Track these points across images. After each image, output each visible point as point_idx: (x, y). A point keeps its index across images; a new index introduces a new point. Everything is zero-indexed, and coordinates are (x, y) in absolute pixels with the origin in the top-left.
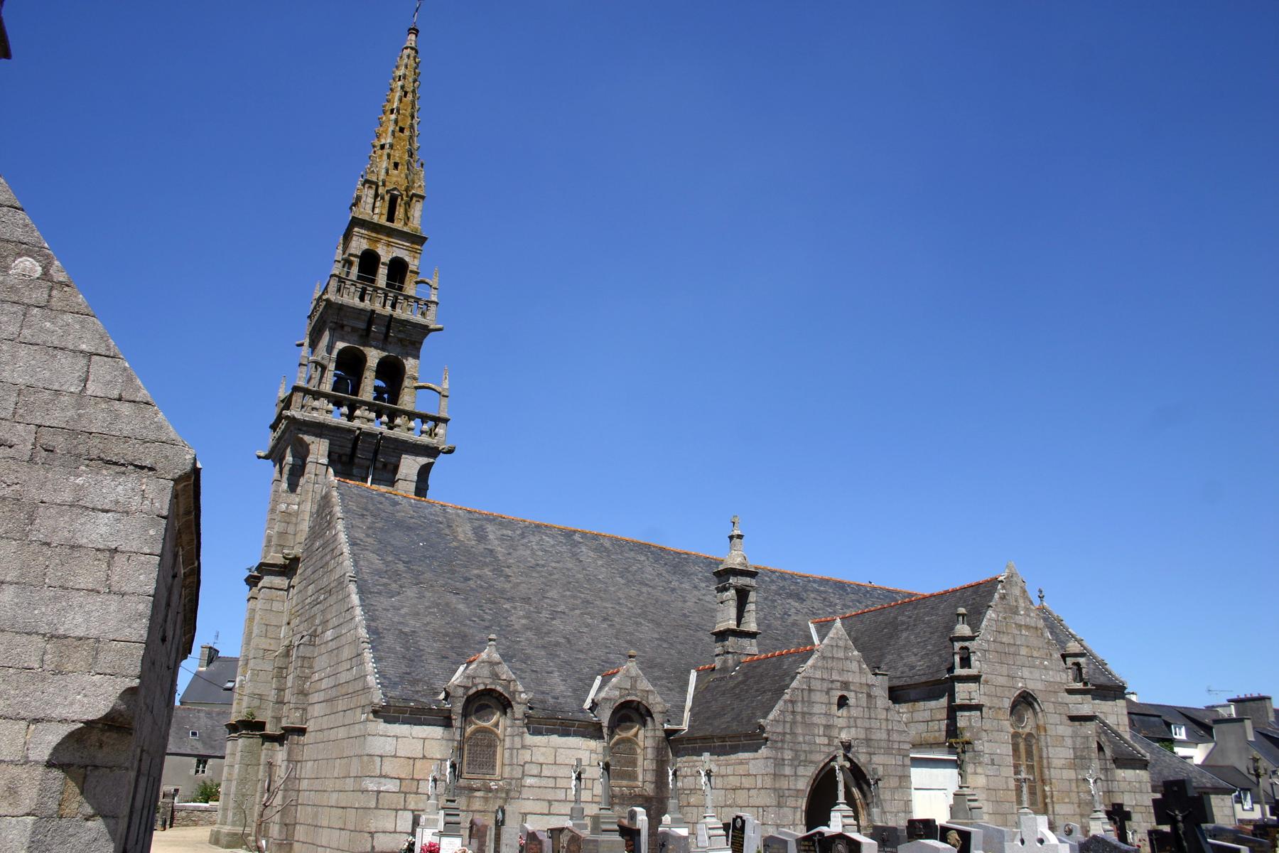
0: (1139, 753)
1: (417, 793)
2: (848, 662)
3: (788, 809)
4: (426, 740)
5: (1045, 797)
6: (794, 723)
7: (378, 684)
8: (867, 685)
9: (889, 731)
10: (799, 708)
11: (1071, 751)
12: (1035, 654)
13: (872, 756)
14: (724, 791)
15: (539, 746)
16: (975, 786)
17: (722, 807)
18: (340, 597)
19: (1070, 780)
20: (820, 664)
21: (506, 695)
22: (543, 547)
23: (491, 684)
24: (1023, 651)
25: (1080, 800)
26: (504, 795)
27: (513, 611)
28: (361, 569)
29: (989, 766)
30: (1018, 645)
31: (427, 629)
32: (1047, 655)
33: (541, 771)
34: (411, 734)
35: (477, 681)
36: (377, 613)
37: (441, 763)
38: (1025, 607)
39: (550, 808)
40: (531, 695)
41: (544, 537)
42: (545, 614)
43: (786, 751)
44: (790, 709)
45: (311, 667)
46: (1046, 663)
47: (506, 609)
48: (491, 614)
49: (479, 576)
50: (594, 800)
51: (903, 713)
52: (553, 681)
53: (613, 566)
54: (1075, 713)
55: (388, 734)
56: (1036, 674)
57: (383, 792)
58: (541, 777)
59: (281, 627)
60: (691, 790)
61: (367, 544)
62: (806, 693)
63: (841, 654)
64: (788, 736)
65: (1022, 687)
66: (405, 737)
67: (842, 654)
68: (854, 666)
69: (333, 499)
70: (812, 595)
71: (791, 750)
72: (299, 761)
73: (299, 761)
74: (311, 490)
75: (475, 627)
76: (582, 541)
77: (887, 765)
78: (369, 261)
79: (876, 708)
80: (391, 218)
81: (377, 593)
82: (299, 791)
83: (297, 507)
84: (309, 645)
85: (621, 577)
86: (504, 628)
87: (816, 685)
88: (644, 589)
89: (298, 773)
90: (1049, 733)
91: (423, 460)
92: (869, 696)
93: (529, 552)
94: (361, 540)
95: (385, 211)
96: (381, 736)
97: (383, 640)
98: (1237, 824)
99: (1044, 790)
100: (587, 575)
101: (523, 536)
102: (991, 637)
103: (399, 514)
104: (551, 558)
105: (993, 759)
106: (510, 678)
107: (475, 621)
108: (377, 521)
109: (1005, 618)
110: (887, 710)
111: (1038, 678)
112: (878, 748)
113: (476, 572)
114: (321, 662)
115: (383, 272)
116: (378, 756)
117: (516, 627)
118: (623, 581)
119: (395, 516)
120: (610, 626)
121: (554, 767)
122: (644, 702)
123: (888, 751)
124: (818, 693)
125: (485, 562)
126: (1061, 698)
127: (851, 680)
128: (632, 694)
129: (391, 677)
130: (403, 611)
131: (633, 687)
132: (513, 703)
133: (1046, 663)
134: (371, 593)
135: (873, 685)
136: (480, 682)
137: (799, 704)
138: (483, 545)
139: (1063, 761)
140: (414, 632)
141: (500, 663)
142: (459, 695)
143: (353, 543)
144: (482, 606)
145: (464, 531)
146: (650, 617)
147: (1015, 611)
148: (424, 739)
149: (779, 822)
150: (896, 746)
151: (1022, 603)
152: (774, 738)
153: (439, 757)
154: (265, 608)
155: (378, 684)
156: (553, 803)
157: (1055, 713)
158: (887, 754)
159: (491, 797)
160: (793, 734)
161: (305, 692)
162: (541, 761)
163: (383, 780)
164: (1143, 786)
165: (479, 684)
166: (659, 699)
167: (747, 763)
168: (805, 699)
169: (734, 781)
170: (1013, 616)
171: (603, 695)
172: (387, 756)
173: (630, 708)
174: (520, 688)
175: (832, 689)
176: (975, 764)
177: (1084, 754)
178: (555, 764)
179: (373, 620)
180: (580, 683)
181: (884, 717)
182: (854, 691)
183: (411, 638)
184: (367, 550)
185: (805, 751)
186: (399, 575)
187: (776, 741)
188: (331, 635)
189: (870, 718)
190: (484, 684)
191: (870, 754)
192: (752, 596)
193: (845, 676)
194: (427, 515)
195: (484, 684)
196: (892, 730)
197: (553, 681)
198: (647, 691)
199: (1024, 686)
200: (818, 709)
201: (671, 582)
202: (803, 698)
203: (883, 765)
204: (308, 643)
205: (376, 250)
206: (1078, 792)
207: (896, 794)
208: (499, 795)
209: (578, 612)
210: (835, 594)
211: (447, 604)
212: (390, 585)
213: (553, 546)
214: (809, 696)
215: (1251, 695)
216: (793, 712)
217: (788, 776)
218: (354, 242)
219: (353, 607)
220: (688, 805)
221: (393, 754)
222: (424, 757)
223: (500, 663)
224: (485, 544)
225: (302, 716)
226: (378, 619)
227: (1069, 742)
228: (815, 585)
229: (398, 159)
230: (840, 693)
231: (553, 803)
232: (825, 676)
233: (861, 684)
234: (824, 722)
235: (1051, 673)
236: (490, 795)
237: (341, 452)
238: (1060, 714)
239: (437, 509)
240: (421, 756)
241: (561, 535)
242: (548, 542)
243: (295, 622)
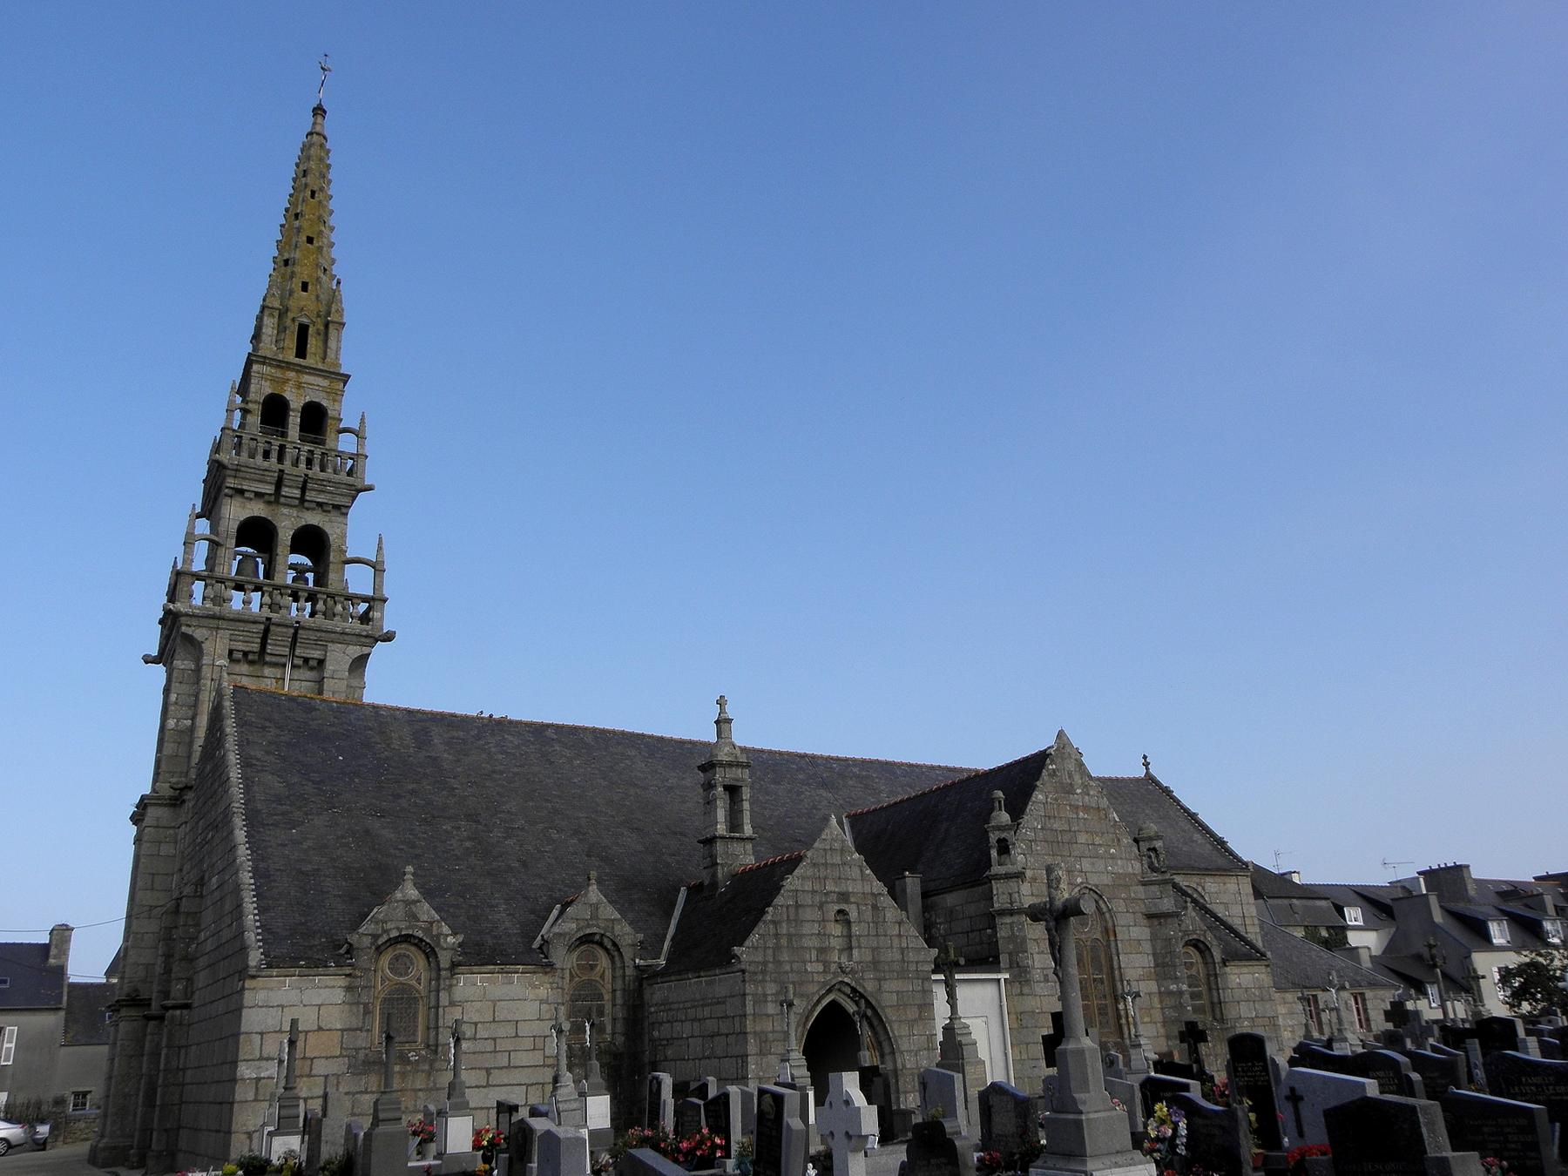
0: (1258, 952)
1: (310, 1076)
2: (847, 868)
3: (773, 1056)
4: (322, 1008)
5: (1119, 1017)
6: (777, 948)
7: (259, 941)
8: (873, 894)
9: (902, 950)
10: (784, 929)
11: (1151, 958)
12: (1098, 840)
13: (882, 982)
14: (701, 1039)
15: (472, 1001)
16: (1022, 1010)
17: (700, 1059)
18: (225, 834)
19: (1150, 994)
20: (809, 873)
21: (428, 941)
22: (505, 748)
23: (407, 928)
24: (1082, 838)
25: (1164, 1018)
26: (427, 1067)
27: (455, 832)
28: (254, 797)
29: (1042, 984)
30: (1075, 832)
31: (337, 864)
33: (476, 1033)
34: (302, 1002)
35: (390, 925)
36: (270, 850)
37: (343, 1034)
38: (1082, 784)
39: (488, 1078)
40: (460, 938)
41: (506, 736)
42: (497, 834)
43: (768, 984)
44: (772, 931)
45: (197, 925)
46: (1112, 851)
47: (446, 831)
48: (424, 838)
49: (413, 792)
50: (546, 1063)
51: (940, 924)
52: (497, 916)
53: (593, 766)
54: (1153, 910)
55: (271, 1004)
56: (1100, 865)
57: (264, 1078)
58: (475, 1039)
59: (173, 875)
60: (668, 1040)
61: (266, 764)
62: (792, 911)
63: (837, 859)
64: (770, 965)
65: (1082, 883)
66: (294, 1006)
67: (839, 858)
68: (856, 873)
69: (224, 711)
70: (850, 783)
71: (775, 982)
72: (183, 1047)
73: (183, 1047)
74: (207, 699)
75: (401, 857)
76: (555, 737)
77: (903, 992)
78: (274, 410)
79: (885, 921)
80: (301, 352)
81: (272, 825)
82: (183, 1085)
83: (190, 721)
84: (194, 896)
85: (604, 778)
86: (439, 854)
87: (807, 899)
88: (632, 791)
89: (181, 1062)
90: (1119, 937)
91: (355, 651)
92: (875, 907)
93: (484, 756)
94: (258, 760)
95: (294, 345)
96: (261, 1007)
97: (273, 884)
99: (1117, 1009)
100: (558, 778)
101: (478, 737)
102: (1038, 824)
103: (315, 722)
104: (514, 761)
105: (1047, 975)
106: (433, 918)
107: (402, 849)
108: (282, 733)
109: (1056, 800)
110: (900, 923)
112: (889, 971)
113: (410, 787)
114: (208, 917)
115: (294, 420)
116: (256, 1033)
117: (457, 852)
118: (604, 783)
119: (310, 725)
120: (580, 840)
121: (493, 1026)
122: (608, 934)
123: (902, 975)
124: (808, 910)
125: (424, 774)
127: (851, 890)
128: (593, 925)
129: (278, 930)
130: (305, 846)
131: (595, 916)
132: (437, 949)
133: (1112, 851)
134: (264, 825)
135: (880, 894)
136: (392, 927)
137: (784, 925)
138: (424, 752)
140: (318, 870)
141: (419, 901)
142: (365, 946)
143: (246, 763)
144: (413, 829)
145: (400, 738)
146: (635, 826)
147: (1070, 790)
148: (319, 1006)
149: (761, 1074)
150: (912, 967)
151: (1077, 779)
152: (752, 969)
153: (339, 1027)
154: (149, 853)
155: (259, 941)
156: (492, 1071)
157: (1127, 912)
158: (901, 978)
159: (410, 1071)
160: (778, 963)
161: (190, 957)
162: (475, 1019)
163: (263, 1063)
164: (1265, 993)
165: (391, 929)
166: (628, 929)
167: (724, 1003)
168: (791, 918)
169: (711, 1025)
170: (1067, 795)
171: (556, 929)
172: (269, 1033)
173: (593, 942)
174: (446, 929)
176: (1020, 983)
177: (1167, 960)
178: (494, 1021)
179: (263, 860)
180: (532, 916)
181: (896, 932)
182: (855, 903)
183: (312, 878)
184: (266, 771)
185: (793, 983)
186: (305, 799)
187: (755, 973)
188: (217, 881)
189: (877, 935)
190: (398, 928)
191: (879, 980)
192: (746, 793)
193: (843, 885)
194: (353, 721)
195: (398, 928)
196: (907, 948)
197: (497, 916)
198: (613, 920)
199: (1085, 881)
200: (807, 929)
201: (667, 780)
202: (788, 917)
203: (897, 992)
204: (192, 894)
205: (283, 394)
206: (1162, 1009)
207: (915, 1027)
208: (420, 1068)
209: (540, 826)
210: (880, 779)
211: (367, 832)
212: (291, 812)
213: (518, 747)
214: (797, 914)
216: (776, 935)
217: (772, 1015)
218: (252, 386)
219: (235, 846)
220: (666, 1060)
221: (277, 1029)
222: (320, 1029)
223: (419, 901)
224: (427, 751)
225: (186, 988)
226: (269, 858)
227: (1147, 947)
228: (855, 770)
229: (306, 277)
230: (837, 908)
231: (492, 1071)
233: (864, 893)
234: (817, 945)
235: (1119, 862)
236: (409, 1068)
237: (247, 649)
238: (1134, 913)
239: (368, 713)
240: (316, 1027)
241: (529, 732)
242: (511, 742)
243: (187, 867)
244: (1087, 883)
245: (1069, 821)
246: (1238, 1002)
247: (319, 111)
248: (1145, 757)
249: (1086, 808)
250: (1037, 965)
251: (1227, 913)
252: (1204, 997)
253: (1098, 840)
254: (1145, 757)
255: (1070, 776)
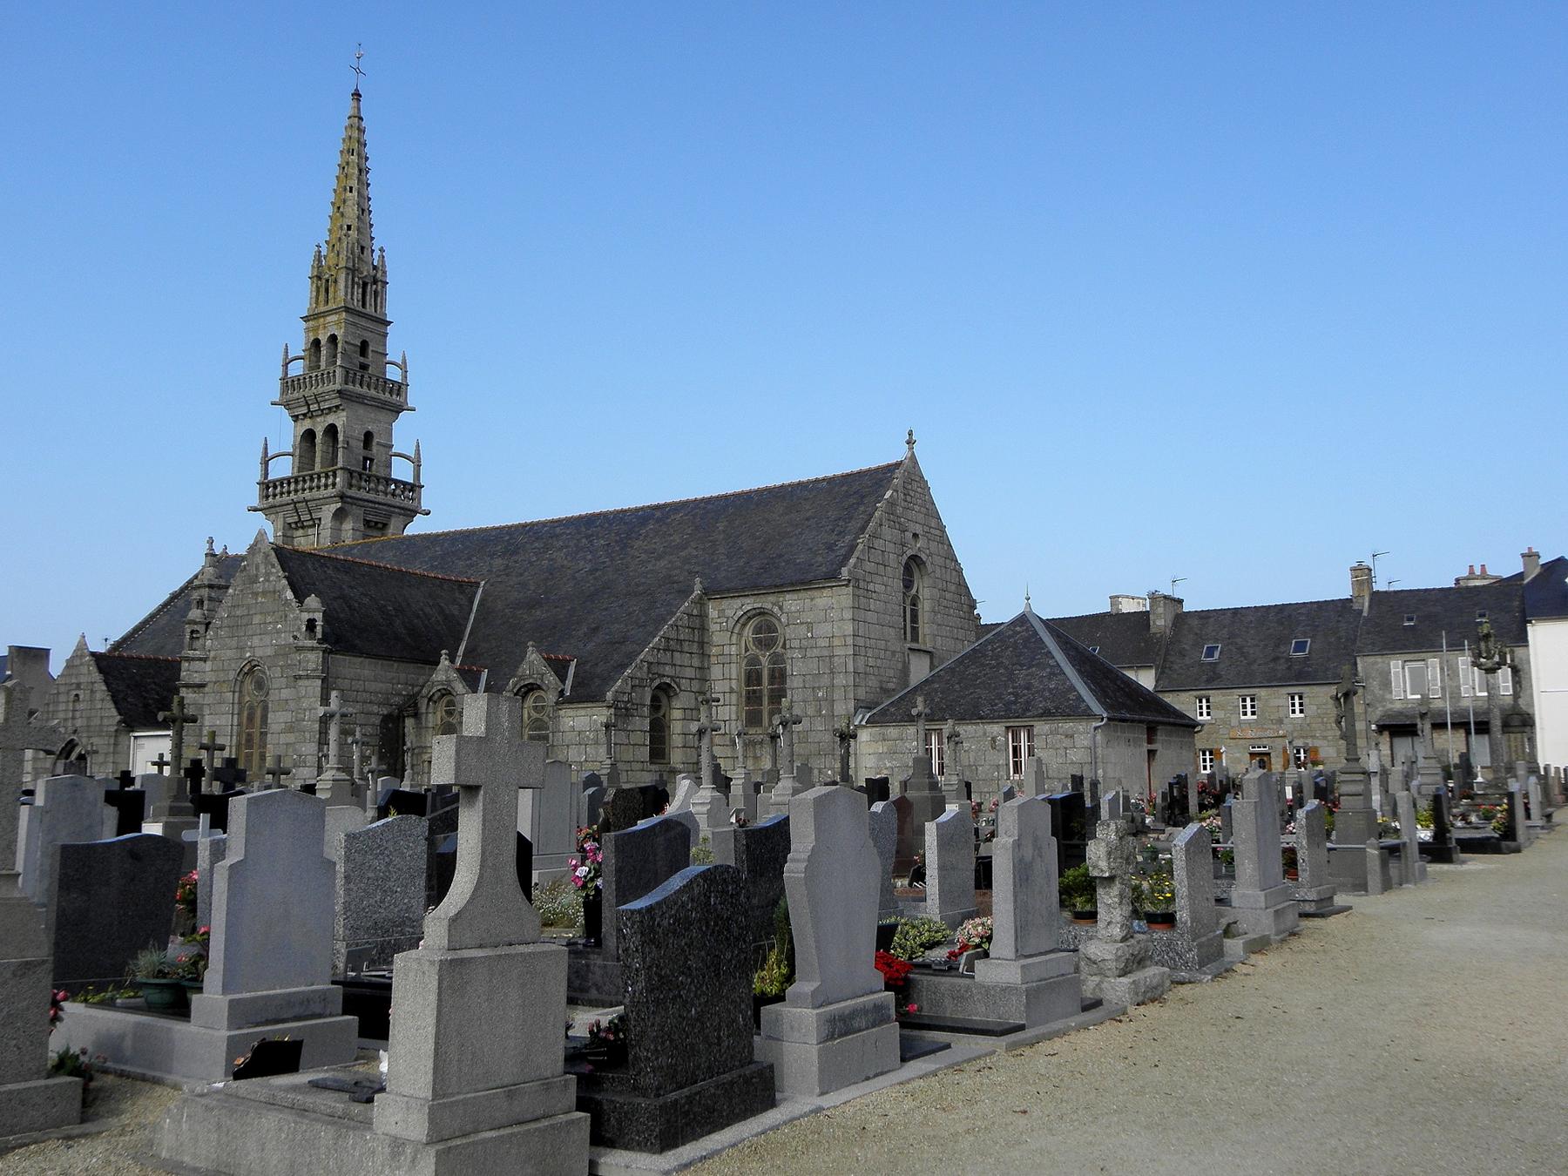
9: (102, 717)
32: (281, 617)
56: (267, 639)
65: (250, 657)
80: (364, 305)
92: (92, 691)
98: (170, 733)
109: (242, 591)
110: (103, 700)
111: (269, 643)
126: (291, 660)
139: (283, 726)
175: (70, 690)
215: (1530, 556)
232: (67, 682)
244: (254, 656)
245: (249, 607)
246: (568, 746)
247: (357, 95)
248: (910, 434)
249: (264, 593)
250: (207, 723)
251: (809, 635)
252: (243, 754)
253: (269, 619)
254: (910, 434)
255: (257, 569)
